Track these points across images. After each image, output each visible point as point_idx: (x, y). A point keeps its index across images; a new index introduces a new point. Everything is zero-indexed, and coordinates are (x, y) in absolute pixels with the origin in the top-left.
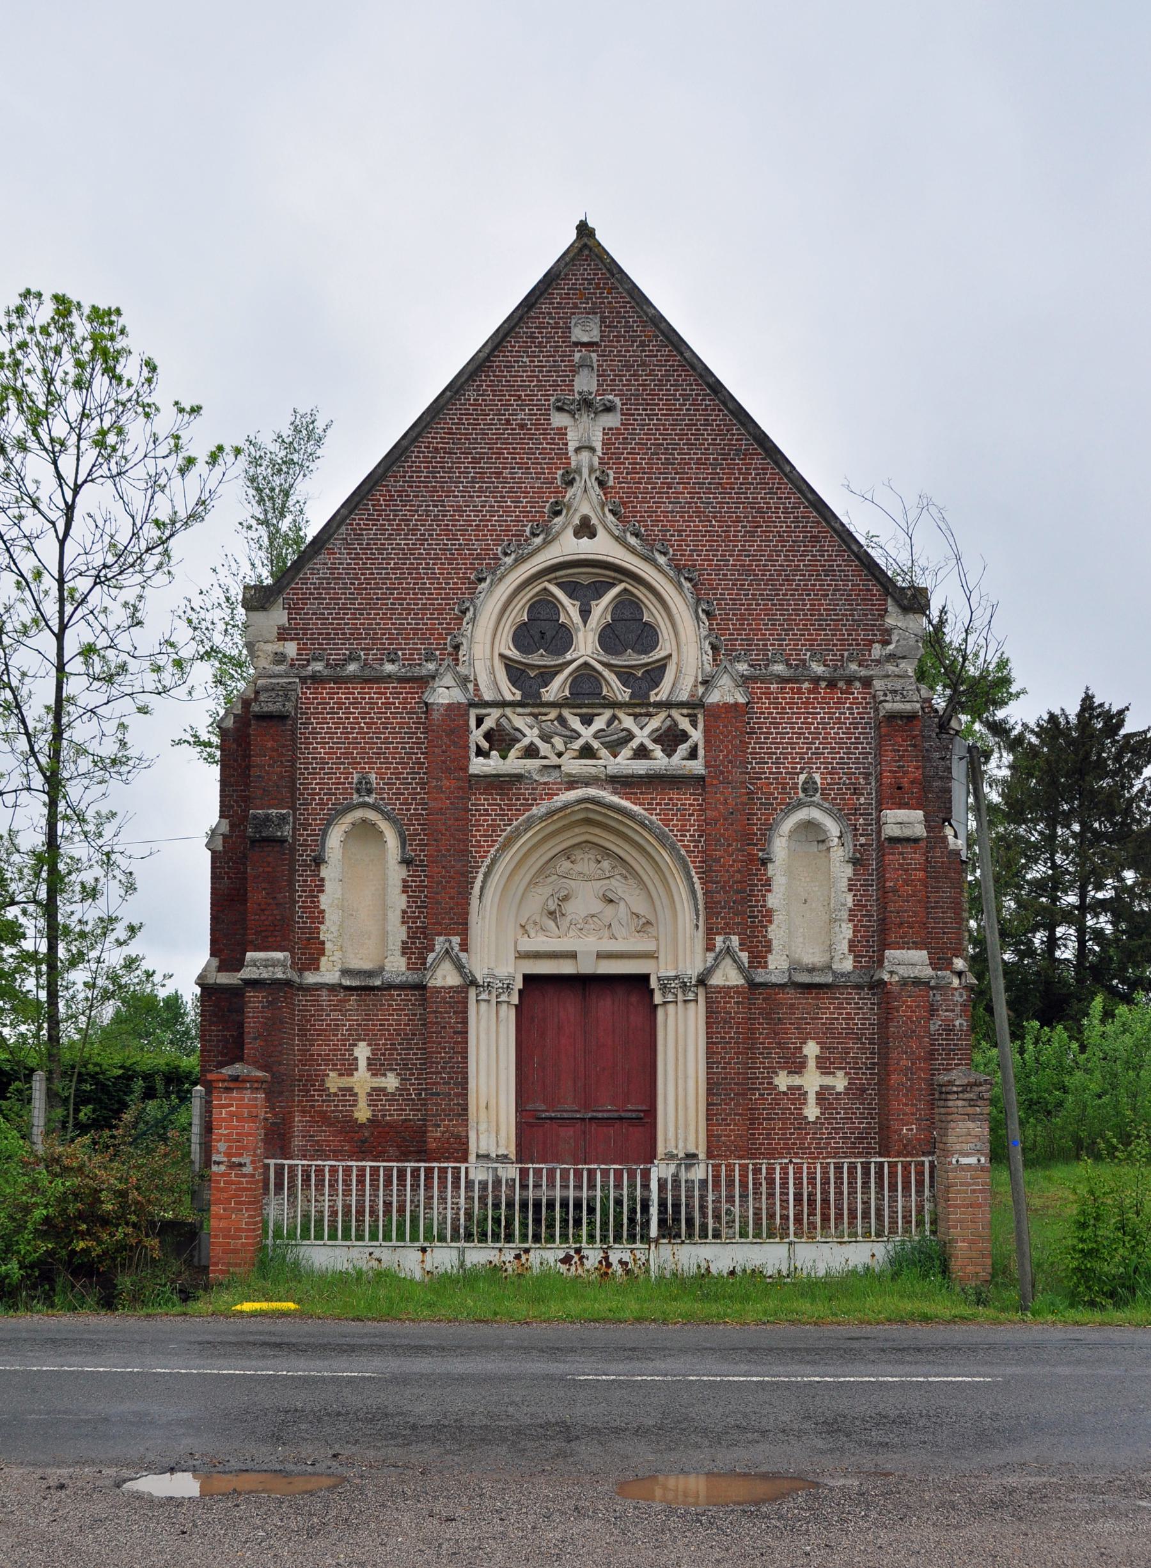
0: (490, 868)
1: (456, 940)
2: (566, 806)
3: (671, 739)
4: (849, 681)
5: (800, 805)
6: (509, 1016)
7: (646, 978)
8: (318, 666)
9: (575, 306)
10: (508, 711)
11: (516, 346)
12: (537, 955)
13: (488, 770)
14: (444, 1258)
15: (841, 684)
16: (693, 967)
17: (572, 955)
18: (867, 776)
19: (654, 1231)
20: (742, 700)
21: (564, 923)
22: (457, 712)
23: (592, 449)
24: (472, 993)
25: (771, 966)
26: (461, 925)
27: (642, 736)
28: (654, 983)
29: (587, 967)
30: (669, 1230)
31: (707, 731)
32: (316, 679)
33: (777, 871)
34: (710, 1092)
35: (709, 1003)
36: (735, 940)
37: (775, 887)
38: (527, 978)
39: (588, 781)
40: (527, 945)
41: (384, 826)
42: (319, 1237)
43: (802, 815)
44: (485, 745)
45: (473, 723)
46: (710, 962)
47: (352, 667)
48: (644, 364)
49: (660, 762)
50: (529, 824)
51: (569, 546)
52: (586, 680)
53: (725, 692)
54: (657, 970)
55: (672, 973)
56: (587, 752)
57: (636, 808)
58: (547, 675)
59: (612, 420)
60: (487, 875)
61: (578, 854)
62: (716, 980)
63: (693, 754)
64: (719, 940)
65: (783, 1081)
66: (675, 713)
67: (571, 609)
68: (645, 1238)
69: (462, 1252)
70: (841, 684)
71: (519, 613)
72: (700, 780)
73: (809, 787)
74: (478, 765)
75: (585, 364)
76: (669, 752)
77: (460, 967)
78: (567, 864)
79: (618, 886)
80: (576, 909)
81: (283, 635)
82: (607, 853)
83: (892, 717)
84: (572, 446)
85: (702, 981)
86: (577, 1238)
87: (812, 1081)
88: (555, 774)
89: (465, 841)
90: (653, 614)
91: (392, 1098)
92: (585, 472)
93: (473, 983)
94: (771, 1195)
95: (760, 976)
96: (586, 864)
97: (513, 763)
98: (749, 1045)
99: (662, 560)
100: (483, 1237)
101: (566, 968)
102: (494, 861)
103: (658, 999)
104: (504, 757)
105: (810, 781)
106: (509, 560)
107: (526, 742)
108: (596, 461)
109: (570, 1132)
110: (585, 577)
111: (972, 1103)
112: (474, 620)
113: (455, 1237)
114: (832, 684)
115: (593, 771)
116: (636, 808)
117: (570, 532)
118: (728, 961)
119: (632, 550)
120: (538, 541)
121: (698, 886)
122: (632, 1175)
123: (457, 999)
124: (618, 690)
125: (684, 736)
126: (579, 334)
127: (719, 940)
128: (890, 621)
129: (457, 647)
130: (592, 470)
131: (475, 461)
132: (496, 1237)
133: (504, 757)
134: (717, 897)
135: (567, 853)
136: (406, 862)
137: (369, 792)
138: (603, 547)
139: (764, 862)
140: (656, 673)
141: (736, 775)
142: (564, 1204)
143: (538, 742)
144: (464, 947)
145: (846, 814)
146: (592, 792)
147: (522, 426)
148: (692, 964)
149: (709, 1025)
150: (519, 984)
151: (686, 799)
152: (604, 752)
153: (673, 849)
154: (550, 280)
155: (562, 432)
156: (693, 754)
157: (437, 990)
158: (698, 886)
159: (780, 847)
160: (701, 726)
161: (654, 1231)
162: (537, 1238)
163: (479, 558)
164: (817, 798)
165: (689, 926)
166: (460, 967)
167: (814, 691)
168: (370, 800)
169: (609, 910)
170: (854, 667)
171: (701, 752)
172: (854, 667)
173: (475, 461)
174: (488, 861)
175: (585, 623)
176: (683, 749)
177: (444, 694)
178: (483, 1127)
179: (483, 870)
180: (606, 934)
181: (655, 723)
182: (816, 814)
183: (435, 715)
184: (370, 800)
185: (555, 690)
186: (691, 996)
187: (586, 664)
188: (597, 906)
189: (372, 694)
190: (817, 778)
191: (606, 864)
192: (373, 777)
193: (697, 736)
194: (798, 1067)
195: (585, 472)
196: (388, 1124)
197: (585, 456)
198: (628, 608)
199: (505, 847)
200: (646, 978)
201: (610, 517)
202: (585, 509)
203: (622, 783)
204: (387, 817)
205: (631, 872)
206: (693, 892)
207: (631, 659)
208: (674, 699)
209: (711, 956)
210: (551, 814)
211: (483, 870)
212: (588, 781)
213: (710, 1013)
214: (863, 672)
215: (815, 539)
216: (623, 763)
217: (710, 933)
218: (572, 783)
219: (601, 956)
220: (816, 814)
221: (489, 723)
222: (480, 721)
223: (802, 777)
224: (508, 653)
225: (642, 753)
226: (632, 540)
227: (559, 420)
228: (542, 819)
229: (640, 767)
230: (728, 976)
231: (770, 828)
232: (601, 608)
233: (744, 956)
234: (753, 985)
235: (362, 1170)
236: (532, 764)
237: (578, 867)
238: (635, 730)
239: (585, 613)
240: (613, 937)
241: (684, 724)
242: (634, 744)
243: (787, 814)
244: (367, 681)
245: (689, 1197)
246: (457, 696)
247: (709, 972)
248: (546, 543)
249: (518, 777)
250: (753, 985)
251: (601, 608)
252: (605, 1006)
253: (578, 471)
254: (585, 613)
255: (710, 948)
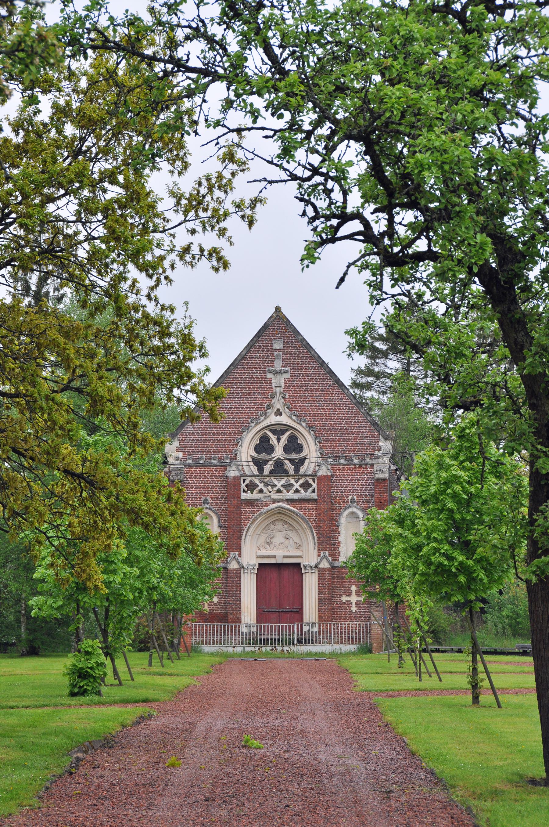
0: (248, 529)
1: (237, 553)
2: (272, 509)
3: (306, 486)
4: (366, 465)
5: (349, 507)
6: (254, 577)
7: (299, 564)
8: (190, 461)
9: (275, 336)
10: (253, 478)
11: (254, 350)
12: (263, 557)
13: (247, 498)
14: (239, 649)
15: (364, 466)
16: (314, 561)
17: (275, 557)
18: (372, 497)
19: (295, 642)
20: (329, 474)
21: (272, 546)
22: (237, 478)
23: (281, 387)
24: (242, 570)
25: (340, 560)
26: (238, 548)
27: (297, 486)
28: (302, 566)
29: (279, 560)
30: (299, 642)
31: (318, 484)
32: (189, 465)
33: (342, 529)
34: (319, 603)
35: (319, 574)
36: (327, 553)
37: (341, 534)
38: (260, 564)
39: (279, 501)
40: (260, 553)
41: (213, 515)
42: (206, 644)
43: (350, 510)
44: (246, 489)
45: (242, 482)
46: (319, 560)
47: (201, 462)
48: (298, 356)
49: (303, 494)
50: (260, 515)
51: (273, 419)
52: (279, 464)
53: (324, 471)
54: (303, 562)
55: (307, 563)
56: (279, 491)
57: (295, 510)
58: (266, 462)
59: (288, 376)
60: (247, 532)
61: (277, 523)
62: (321, 566)
63: (314, 491)
64: (322, 553)
65: (344, 599)
66: (308, 478)
67: (273, 439)
68: (293, 644)
69: (244, 648)
70: (364, 466)
71: (257, 441)
72: (316, 500)
73: (353, 501)
74: (244, 496)
75: (278, 357)
76: (306, 491)
77: (238, 562)
78: (273, 526)
79: (290, 533)
80: (276, 541)
81: (178, 450)
82: (286, 522)
83: (378, 480)
84: (274, 385)
85: (316, 566)
86: (275, 644)
87: (354, 599)
88: (269, 498)
89: (240, 517)
90: (301, 441)
91: (216, 605)
92: (278, 395)
93: (243, 567)
94: (341, 637)
95: (336, 564)
96: (279, 526)
97: (255, 495)
98: (332, 587)
99: (304, 424)
100: (250, 644)
101: (273, 561)
102: (249, 527)
103: (303, 571)
104: (252, 493)
105: (353, 499)
106: (253, 425)
107: (259, 488)
108: (282, 390)
109: (275, 616)
110: (278, 428)
111: (377, 607)
112: (241, 445)
113: (242, 644)
114: (360, 466)
115: (281, 498)
116: (295, 510)
117: (273, 414)
118: (325, 560)
119: (294, 421)
120: (262, 418)
121: (315, 535)
122: (290, 626)
123: (238, 573)
124: (290, 468)
125: (310, 486)
126: (276, 346)
127: (322, 553)
128: (381, 444)
129: (236, 454)
130: (280, 393)
131: (241, 390)
132: (253, 644)
133: (252, 493)
134: (321, 539)
135: (273, 523)
136: (220, 527)
137: (208, 504)
138: (284, 419)
139: (338, 526)
140: (302, 461)
141: (328, 498)
142: (271, 639)
143: (263, 488)
144: (240, 556)
145: (364, 510)
146: (281, 504)
147: (257, 378)
148: (314, 560)
149: (319, 581)
150: (257, 567)
151: (312, 506)
152: (285, 491)
153: (307, 523)
154: (265, 327)
155: (270, 380)
156: (314, 491)
157: (231, 570)
158: (315, 535)
159: (343, 520)
160: (316, 482)
161: (295, 642)
162: (264, 644)
163: (243, 423)
164: (355, 504)
165: (312, 548)
166: (238, 562)
167: (355, 468)
168: (208, 506)
169: (287, 541)
170: (368, 460)
171: (316, 491)
172: (368, 460)
173: (241, 390)
174: (247, 527)
175: (279, 442)
176: (310, 490)
177: (233, 472)
178: (246, 614)
179: (246, 530)
180: (286, 549)
181: (301, 482)
182: (355, 510)
183: (230, 480)
184: (208, 506)
185: (268, 468)
186: (313, 571)
187: (279, 459)
188: (283, 540)
189: (208, 470)
190: (355, 498)
191: (286, 526)
192: (209, 498)
193: (315, 485)
194: (349, 594)
195: (278, 395)
196: (215, 614)
197: (278, 389)
198: (293, 439)
199: (252, 523)
200: (299, 564)
201: (287, 410)
202: (278, 406)
203: (291, 501)
204: (213, 511)
205: (294, 529)
206: (314, 537)
207: (294, 456)
208: (306, 473)
209: (319, 558)
210: (267, 512)
211: (246, 530)
212: (279, 501)
213: (319, 577)
214: (371, 462)
215: (355, 415)
216: (291, 495)
217: (319, 550)
218: (274, 501)
219: (284, 557)
220: (355, 510)
221: (247, 482)
222: (244, 481)
223: (350, 497)
224: (253, 455)
225: (297, 491)
226: (294, 418)
227: (269, 376)
228: (264, 514)
229: (296, 496)
230: (325, 565)
231: (340, 514)
232: (284, 438)
233: (330, 558)
234: (333, 567)
235: (210, 626)
236: (261, 495)
237: (276, 527)
238: (295, 484)
239: (279, 440)
240: (288, 551)
241: (311, 482)
242: (294, 488)
243: (345, 510)
244: (206, 466)
245: (312, 637)
246: (237, 473)
247: (318, 563)
248: (265, 418)
249: (257, 500)
250: (333, 567)
251: (284, 438)
252: (286, 573)
253: (276, 394)
254: (279, 440)
255: (319, 555)
